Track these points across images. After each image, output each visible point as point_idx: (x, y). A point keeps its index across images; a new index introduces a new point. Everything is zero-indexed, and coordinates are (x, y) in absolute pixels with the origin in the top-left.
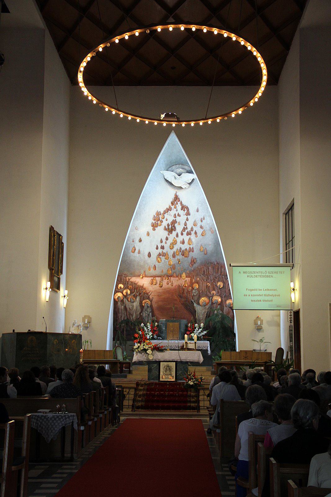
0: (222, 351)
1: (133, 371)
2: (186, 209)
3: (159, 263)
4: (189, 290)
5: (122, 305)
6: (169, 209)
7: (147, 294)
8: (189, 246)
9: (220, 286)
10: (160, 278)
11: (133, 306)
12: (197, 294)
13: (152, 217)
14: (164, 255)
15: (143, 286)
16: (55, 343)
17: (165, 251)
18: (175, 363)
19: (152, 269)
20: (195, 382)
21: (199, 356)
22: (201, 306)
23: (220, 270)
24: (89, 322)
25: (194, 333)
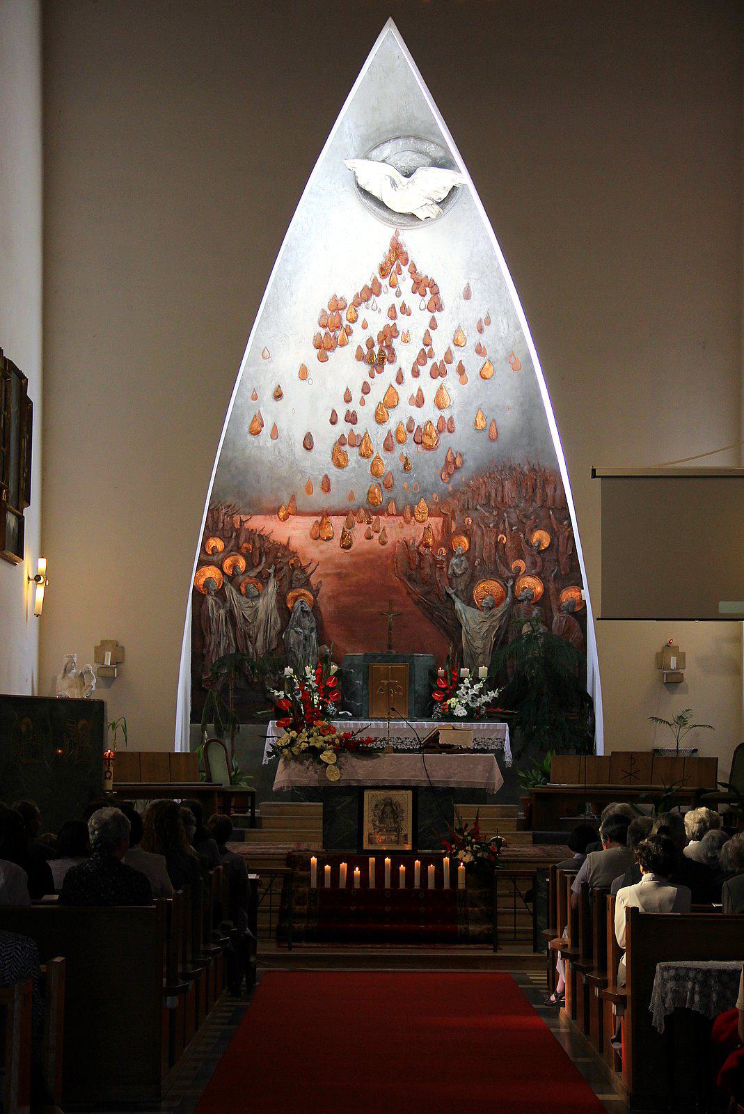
0: (549, 754)
1: (263, 821)
2: (428, 289)
3: (340, 471)
4: (440, 558)
5: (219, 608)
6: (372, 291)
7: (303, 570)
8: (438, 413)
9: (540, 542)
10: (343, 518)
11: (256, 612)
12: (466, 569)
13: (316, 317)
14: (358, 442)
15: (288, 543)
16: (24, 728)
17: (359, 429)
18: (410, 793)
19: (317, 489)
20: (479, 855)
21: (490, 771)
22: (478, 609)
23: (539, 492)
24: (117, 662)
25: (456, 696)
